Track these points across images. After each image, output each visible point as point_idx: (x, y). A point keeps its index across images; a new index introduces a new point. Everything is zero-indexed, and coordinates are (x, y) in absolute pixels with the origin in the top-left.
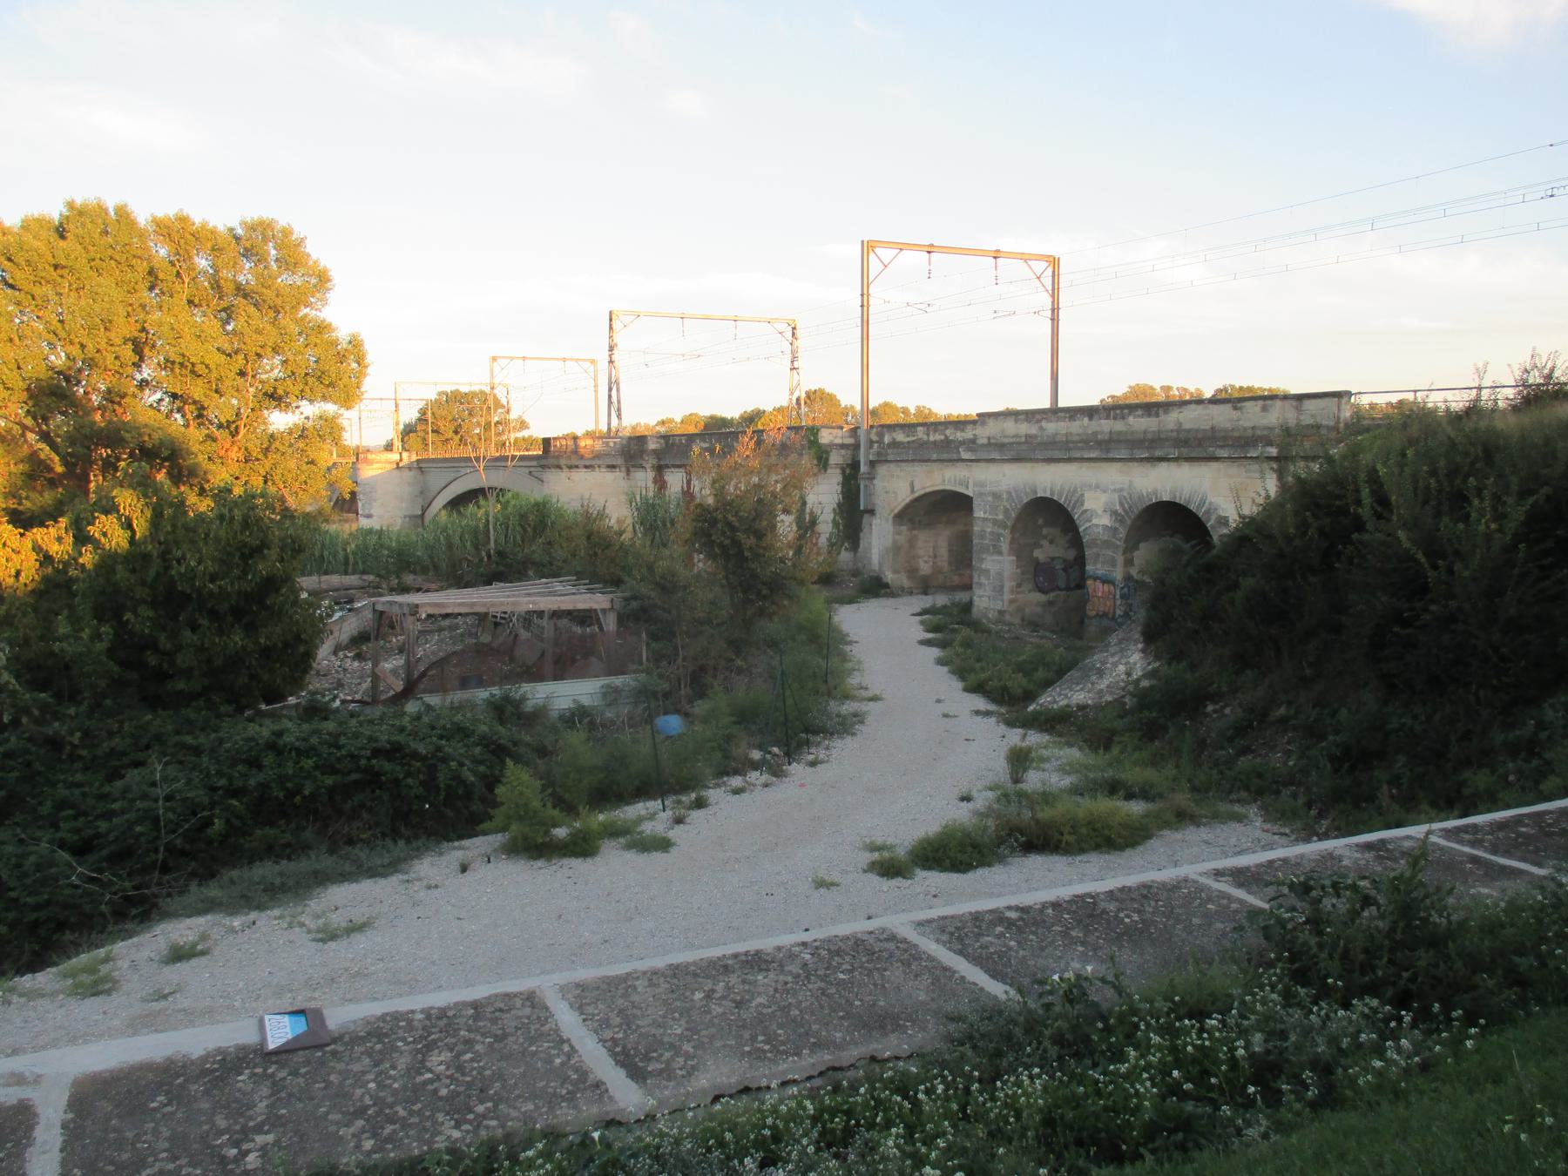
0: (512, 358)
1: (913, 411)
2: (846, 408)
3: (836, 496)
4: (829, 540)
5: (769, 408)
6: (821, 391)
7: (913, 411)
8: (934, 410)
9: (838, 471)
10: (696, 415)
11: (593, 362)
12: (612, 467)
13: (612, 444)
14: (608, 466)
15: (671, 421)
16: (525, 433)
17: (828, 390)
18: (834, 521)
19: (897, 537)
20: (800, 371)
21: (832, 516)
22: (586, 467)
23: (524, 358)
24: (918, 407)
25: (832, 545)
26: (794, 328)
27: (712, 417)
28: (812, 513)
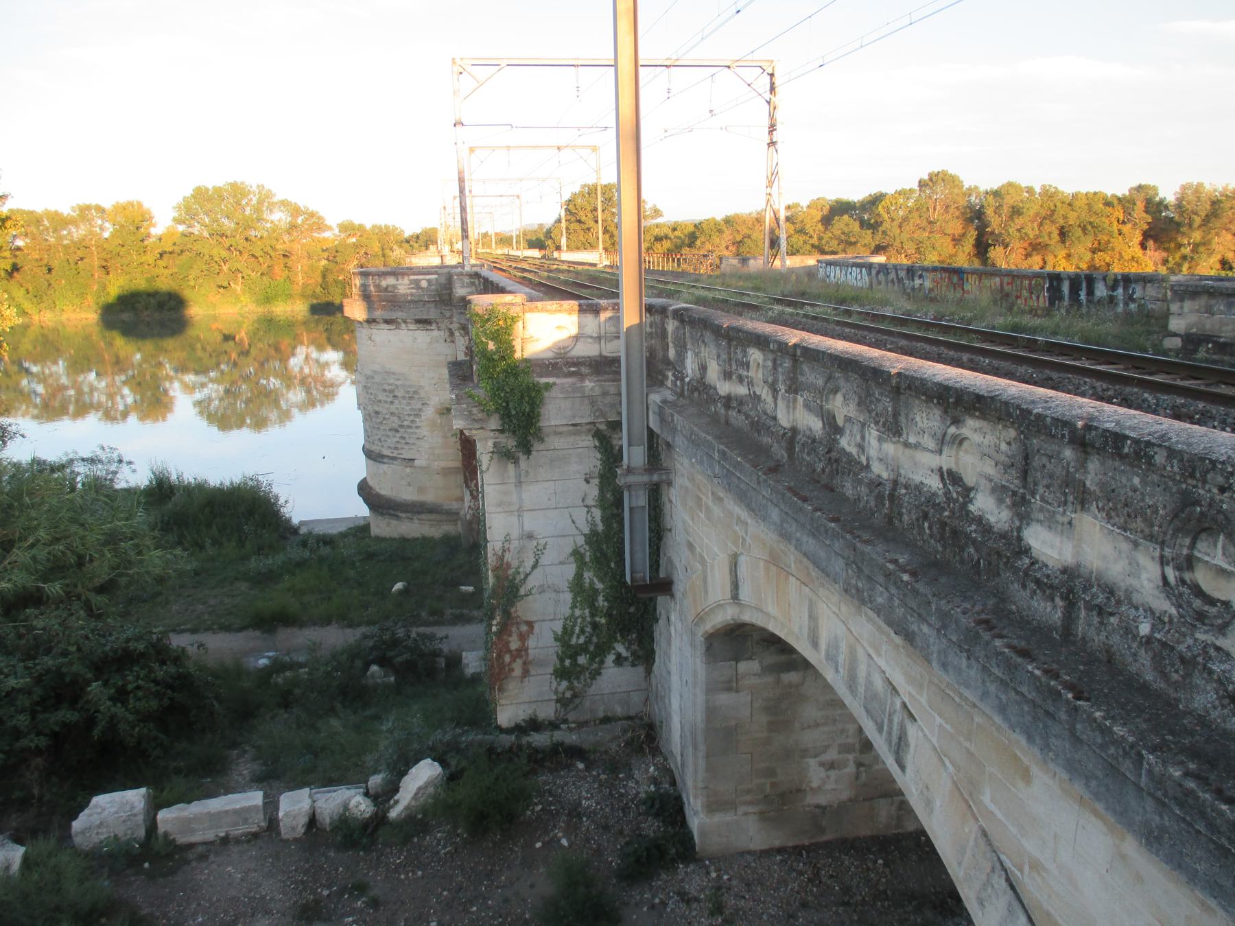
0: (493, 149)
1: (1038, 190)
2: (970, 189)
3: (581, 515)
4: (563, 638)
5: (889, 189)
6: (944, 173)
7: (1038, 190)
8: (1061, 188)
9: (588, 441)
10: (823, 199)
11: (594, 149)
12: (424, 322)
13: (424, 284)
14: (418, 321)
15: (797, 205)
16: (659, 220)
17: (952, 171)
18: (577, 586)
19: (724, 699)
20: (779, 146)
21: (570, 570)
22: (387, 322)
23: (508, 148)
24: (1044, 186)
25: (568, 650)
26: (772, 75)
27: (837, 202)
28: (502, 566)
